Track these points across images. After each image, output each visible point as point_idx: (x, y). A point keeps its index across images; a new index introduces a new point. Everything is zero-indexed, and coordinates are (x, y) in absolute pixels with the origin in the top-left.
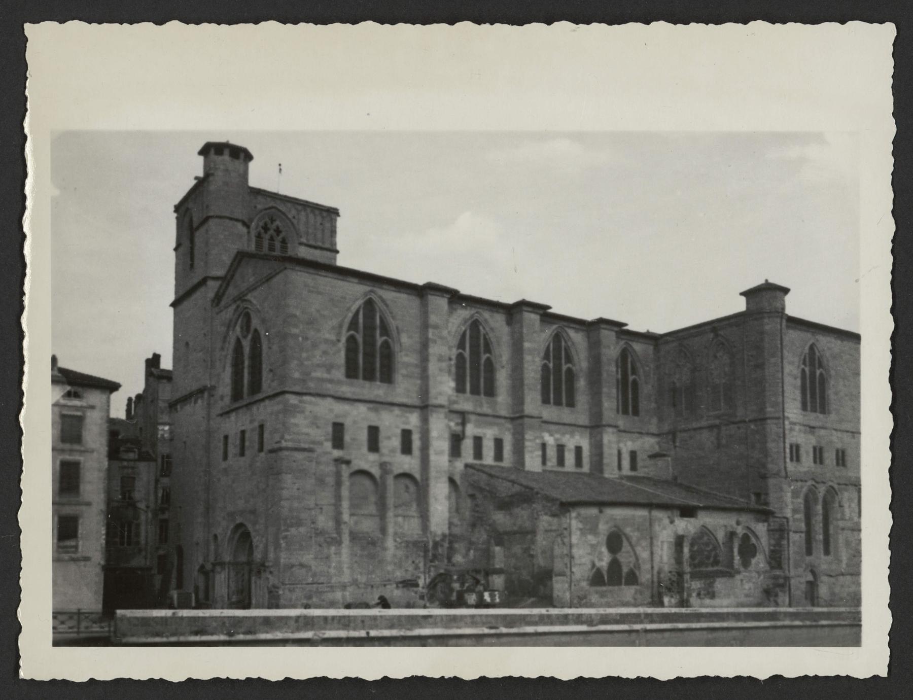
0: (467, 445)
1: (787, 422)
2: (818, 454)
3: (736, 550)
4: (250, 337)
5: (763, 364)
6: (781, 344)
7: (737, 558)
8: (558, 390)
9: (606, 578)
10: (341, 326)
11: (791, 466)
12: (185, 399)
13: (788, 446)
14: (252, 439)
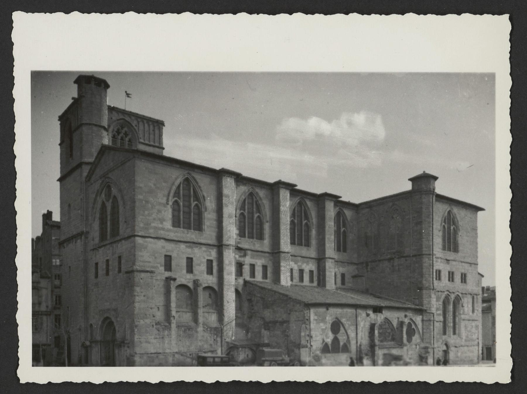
0: (246, 269)
2: (451, 276)
3: (405, 332)
4: (111, 201)
5: (421, 222)
7: (405, 336)
8: (300, 236)
9: (330, 348)
10: (169, 195)
11: (436, 282)
12: (69, 240)
13: (434, 271)
14: (114, 264)
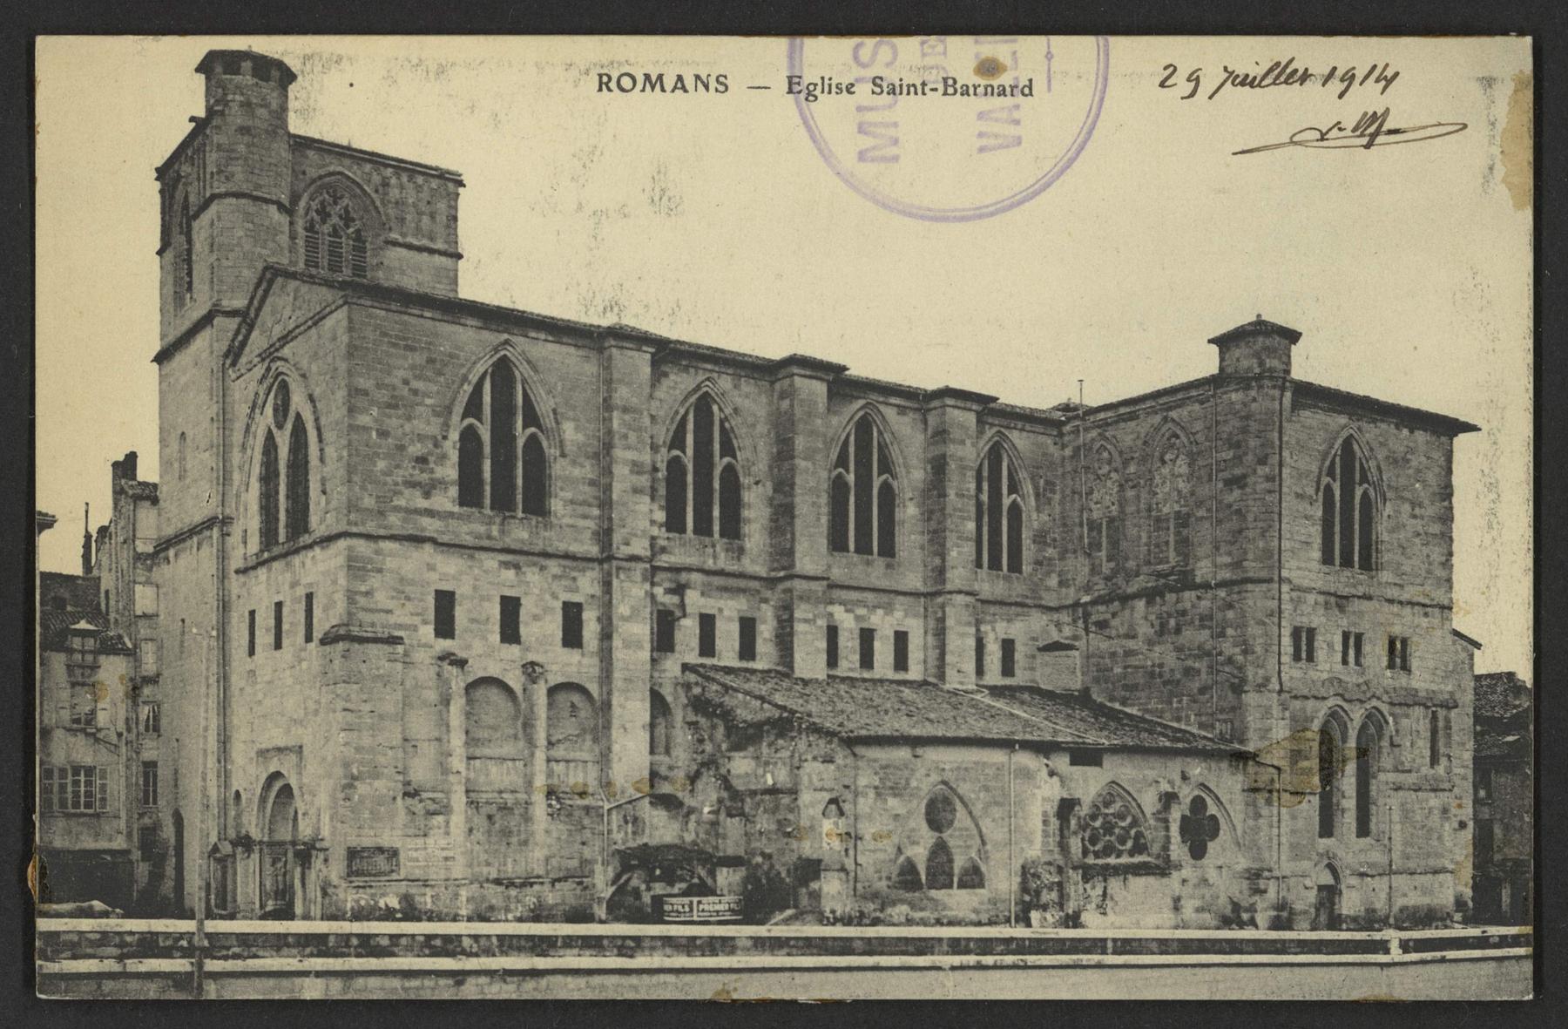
0: (688, 630)
1: (1285, 588)
2: (1353, 643)
4: (289, 426)
6: (1280, 439)
9: (923, 878)
10: (449, 410)
14: (294, 617)
